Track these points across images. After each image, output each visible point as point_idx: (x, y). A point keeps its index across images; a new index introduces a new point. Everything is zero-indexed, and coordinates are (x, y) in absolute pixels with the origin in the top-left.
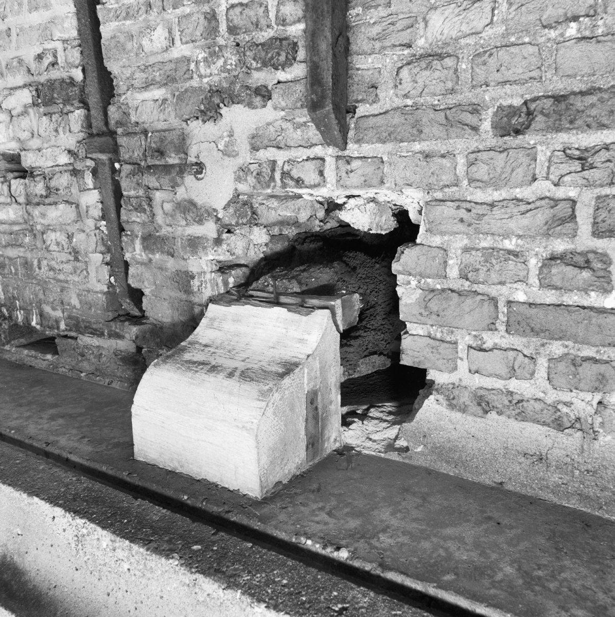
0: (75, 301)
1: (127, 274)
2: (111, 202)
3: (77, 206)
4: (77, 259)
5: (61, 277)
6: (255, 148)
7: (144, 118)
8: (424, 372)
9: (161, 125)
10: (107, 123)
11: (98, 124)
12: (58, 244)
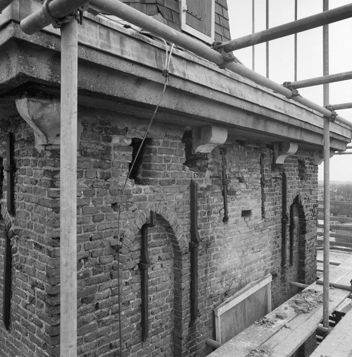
0: (232, 151)
2: (224, 172)
6: (202, 180)
9: (215, 185)
10: (224, 187)
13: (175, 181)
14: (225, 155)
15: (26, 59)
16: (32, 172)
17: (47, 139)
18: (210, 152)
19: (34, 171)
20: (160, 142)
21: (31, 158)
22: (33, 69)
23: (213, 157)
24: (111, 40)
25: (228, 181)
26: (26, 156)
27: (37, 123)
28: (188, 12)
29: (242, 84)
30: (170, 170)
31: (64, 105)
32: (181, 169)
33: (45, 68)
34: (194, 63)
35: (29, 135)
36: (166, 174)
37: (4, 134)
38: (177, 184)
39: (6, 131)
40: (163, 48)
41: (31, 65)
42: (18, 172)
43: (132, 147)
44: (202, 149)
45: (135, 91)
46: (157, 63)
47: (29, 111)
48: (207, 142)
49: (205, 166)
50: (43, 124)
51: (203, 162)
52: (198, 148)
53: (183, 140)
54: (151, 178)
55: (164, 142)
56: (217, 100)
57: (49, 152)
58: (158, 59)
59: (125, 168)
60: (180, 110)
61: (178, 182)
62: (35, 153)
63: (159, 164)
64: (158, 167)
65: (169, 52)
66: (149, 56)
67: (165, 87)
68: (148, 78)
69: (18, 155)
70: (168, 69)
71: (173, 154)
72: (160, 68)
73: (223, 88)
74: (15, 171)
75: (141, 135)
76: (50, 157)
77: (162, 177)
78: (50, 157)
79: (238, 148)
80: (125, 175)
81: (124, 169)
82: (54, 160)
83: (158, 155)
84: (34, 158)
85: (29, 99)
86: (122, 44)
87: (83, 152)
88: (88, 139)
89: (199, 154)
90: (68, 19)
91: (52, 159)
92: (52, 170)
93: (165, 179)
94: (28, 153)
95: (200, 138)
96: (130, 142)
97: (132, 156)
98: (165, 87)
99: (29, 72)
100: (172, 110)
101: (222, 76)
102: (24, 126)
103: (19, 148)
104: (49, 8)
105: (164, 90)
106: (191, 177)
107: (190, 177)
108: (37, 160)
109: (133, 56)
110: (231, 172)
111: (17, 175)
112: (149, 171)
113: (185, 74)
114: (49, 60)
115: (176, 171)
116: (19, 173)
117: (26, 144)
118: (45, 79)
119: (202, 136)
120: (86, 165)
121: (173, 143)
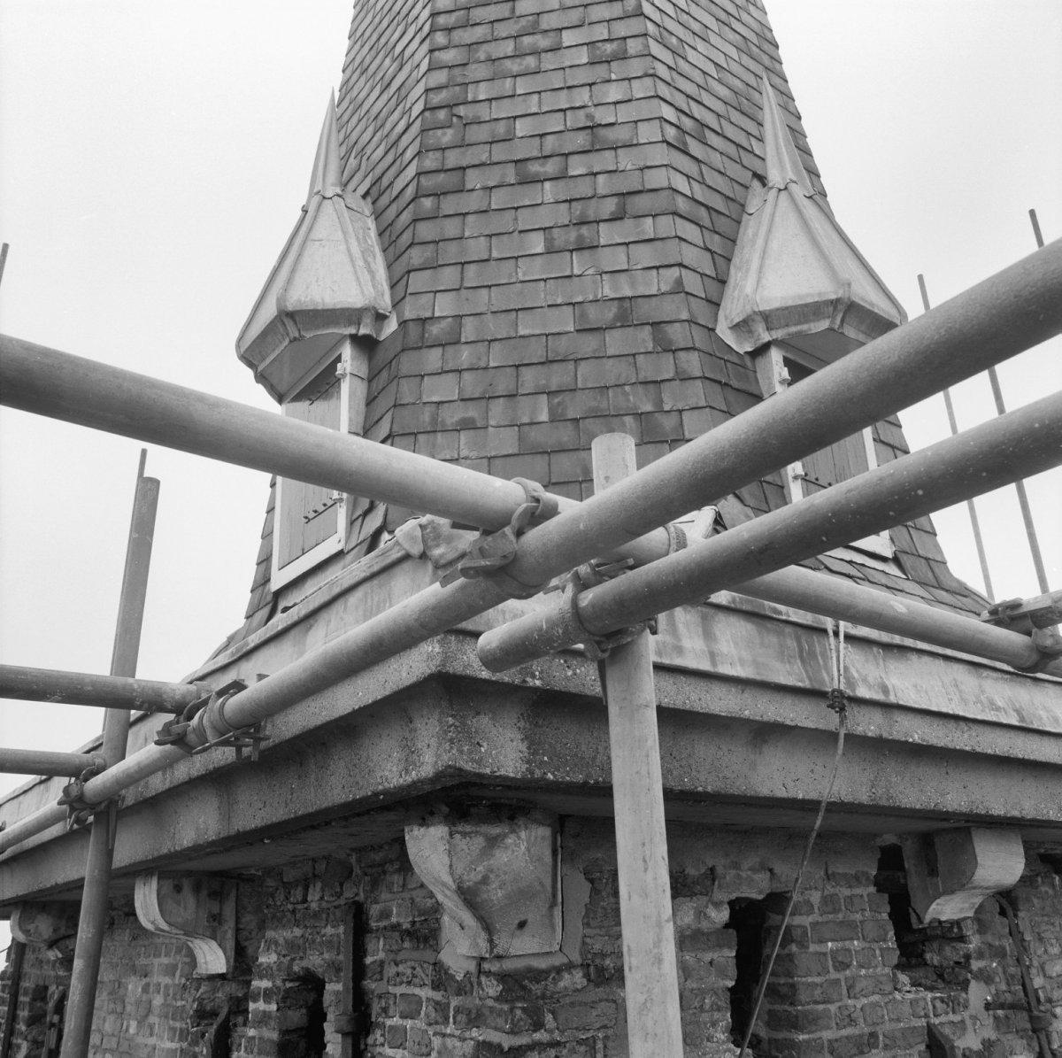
0: (1035, 901)
1: (1010, 930)
2: (1027, 981)
3: (1045, 976)
4: (1039, 934)
5: (1046, 919)
6: (963, 1021)
7: (1020, 1042)
8: (878, 891)
9: (1010, 1037)
10: (1038, 1037)
11: (1043, 1037)
12: (1052, 945)
13: (878, 1037)
14: (1016, 916)
15: (463, 724)
16: (429, 1044)
17: (491, 941)
18: (971, 914)
19: (437, 1042)
20: (812, 899)
21: (425, 993)
22: (483, 750)
23: (982, 927)
24: (681, 628)
25: (1048, 1015)
26: (409, 983)
27: (469, 896)
28: (807, 478)
29: (1047, 685)
30: (855, 998)
31: (635, 898)
32: (888, 988)
33: (512, 741)
34: (902, 649)
35: (419, 915)
36: (846, 1013)
37: (330, 902)
38: (886, 1047)
39: (339, 895)
40: (815, 625)
41: (477, 740)
42: (378, 1036)
43: (733, 932)
44: (947, 909)
45: (753, 766)
46: (807, 672)
47: (451, 866)
48: (959, 880)
49: (957, 963)
50: (485, 896)
51: (948, 950)
52: (934, 906)
53: (880, 885)
54: (801, 1037)
55: (826, 900)
56: (989, 751)
57: (495, 983)
58: (807, 658)
59: (719, 1009)
60: (884, 802)
61: (887, 1042)
62: (441, 978)
63: (818, 980)
64: (818, 992)
65: (836, 634)
66: (782, 655)
67: (841, 741)
68: (788, 722)
69: (378, 976)
70: (842, 688)
71: (858, 939)
72: (817, 686)
73: (998, 709)
74: (367, 1034)
75: (755, 888)
76: (497, 999)
77: (834, 1025)
78: (497, 999)
79: (1053, 886)
80: (722, 1037)
81: (717, 1015)
82: (512, 1010)
83: (813, 948)
84: (438, 996)
85: (453, 828)
86: (708, 635)
87: (592, 968)
88: (606, 923)
89: (937, 924)
90: (632, 632)
91: (506, 1007)
92: (506, 1047)
93: (844, 1032)
94: (414, 976)
95: (933, 872)
96: (721, 916)
97: (735, 961)
98: (841, 741)
99: (473, 761)
100: (861, 805)
101: (985, 673)
102: (401, 883)
103: (381, 955)
104: (580, 611)
105: (840, 752)
106: (926, 1016)
107: (922, 1013)
108: (449, 1004)
109: (742, 665)
110: (1051, 978)
111: (375, 1045)
112: (790, 1009)
113: (885, 690)
114: (522, 714)
115: (875, 998)
116: (381, 1040)
117: (407, 944)
118: (512, 775)
119: (942, 866)
120: (605, 1014)
121: (851, 898)
